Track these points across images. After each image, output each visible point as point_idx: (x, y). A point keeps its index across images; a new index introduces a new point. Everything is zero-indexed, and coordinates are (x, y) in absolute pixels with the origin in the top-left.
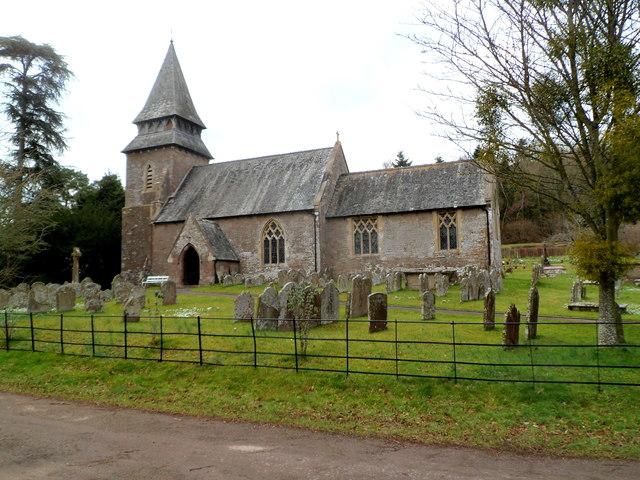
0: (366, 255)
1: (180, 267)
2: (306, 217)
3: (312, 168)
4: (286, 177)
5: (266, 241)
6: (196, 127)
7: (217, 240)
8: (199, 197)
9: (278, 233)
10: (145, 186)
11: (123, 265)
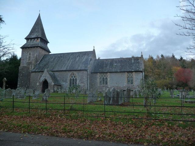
0: (103, 85)
1: (41, 86)
2: (85, 72)
3: (86, 57)
4: (77, 59)
5: (71, 79)
6: (46, 42)
7: (54, 78)
8: (47, 64)
9: (75, 77)
10: (28, 60)
11: (18, 86)
